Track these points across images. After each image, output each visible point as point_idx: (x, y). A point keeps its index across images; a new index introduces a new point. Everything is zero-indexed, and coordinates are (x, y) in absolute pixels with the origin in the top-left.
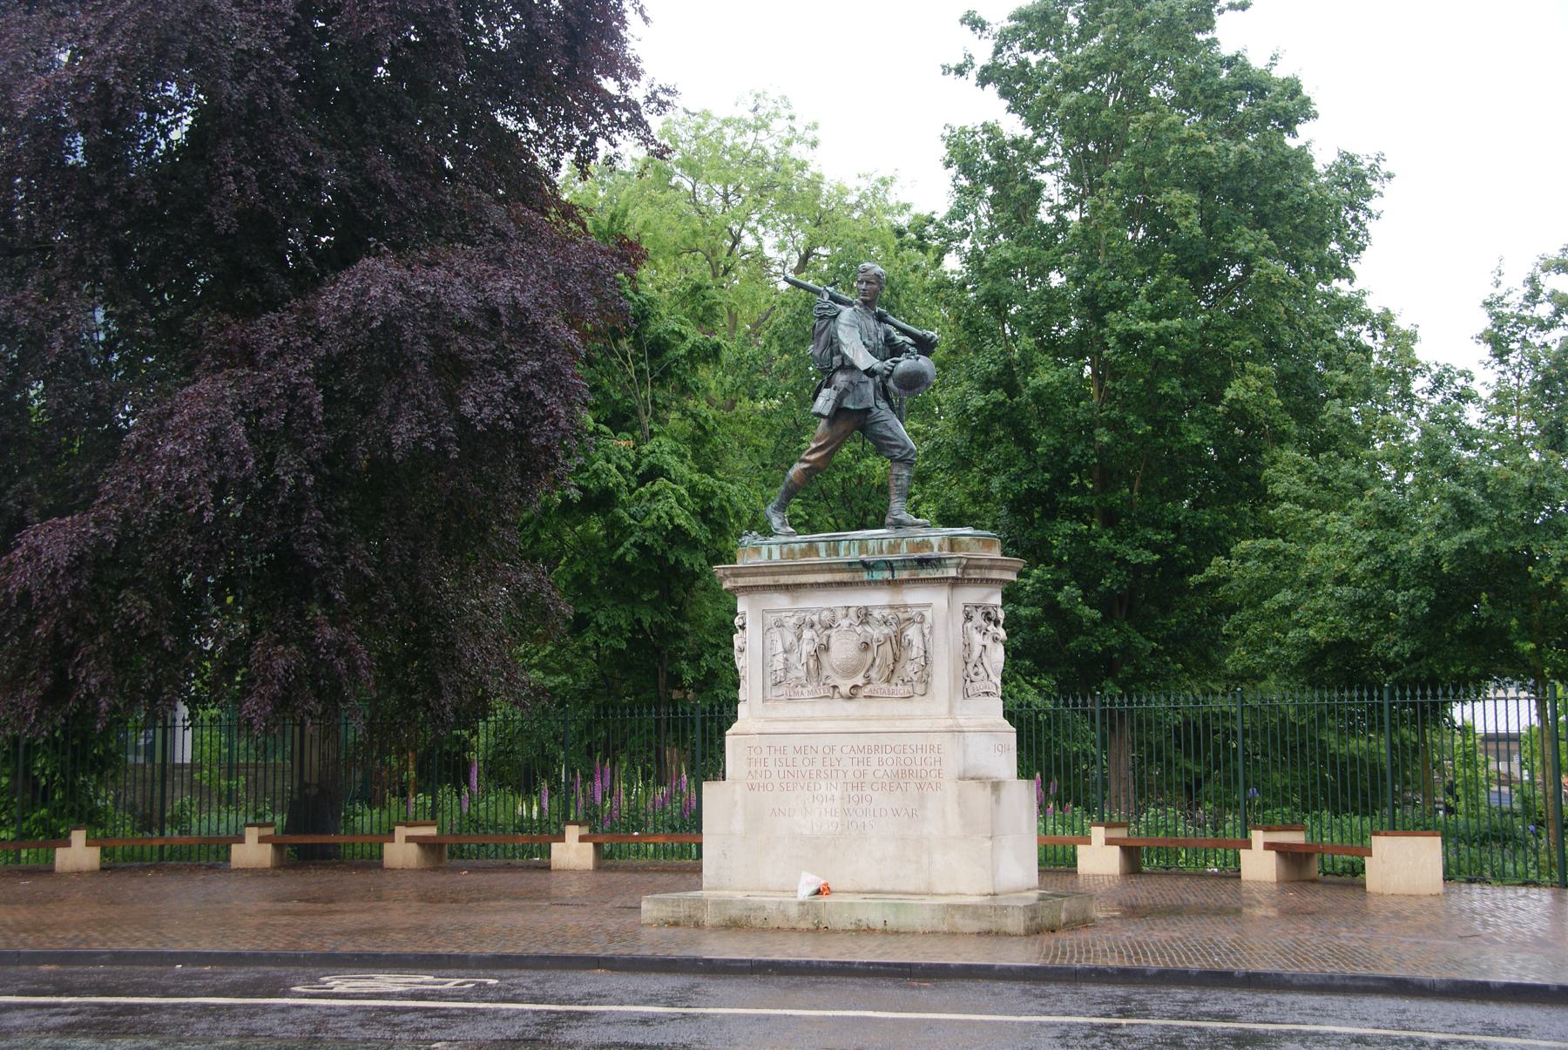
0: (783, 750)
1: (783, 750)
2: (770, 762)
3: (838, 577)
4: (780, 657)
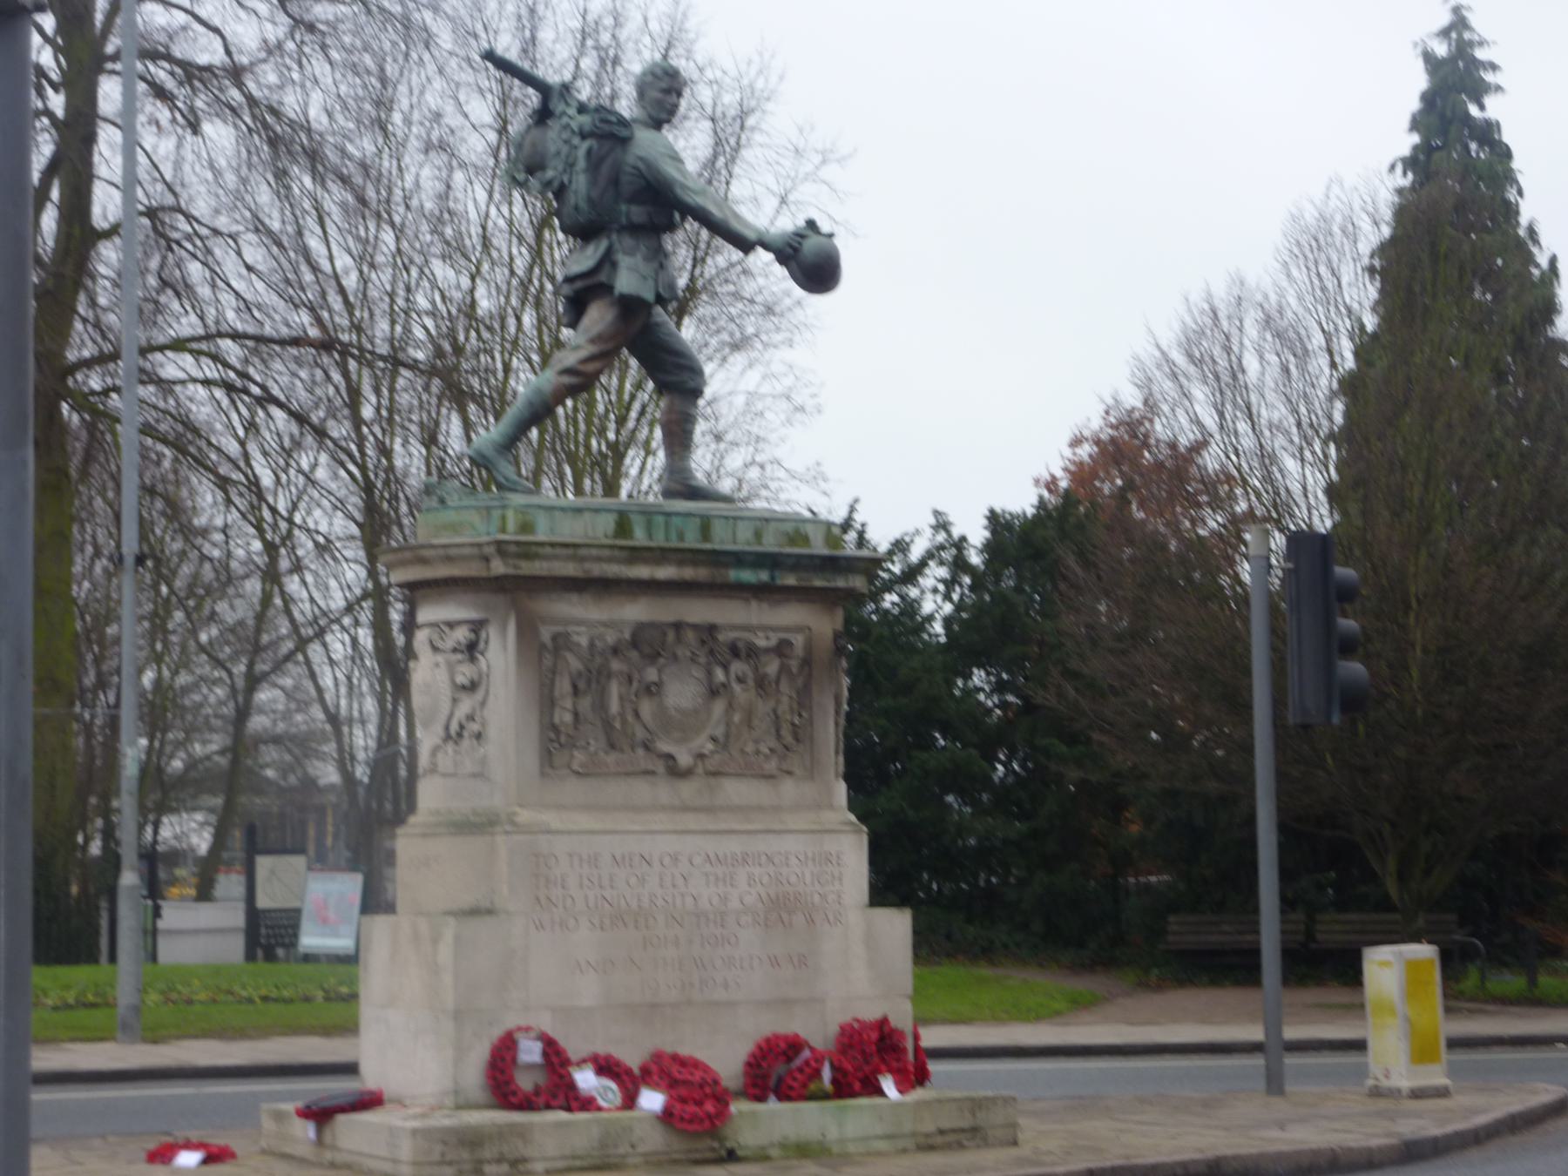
0: (594, 861)
1: (594, 861)
3: (688, 573)
4: (568, 704)
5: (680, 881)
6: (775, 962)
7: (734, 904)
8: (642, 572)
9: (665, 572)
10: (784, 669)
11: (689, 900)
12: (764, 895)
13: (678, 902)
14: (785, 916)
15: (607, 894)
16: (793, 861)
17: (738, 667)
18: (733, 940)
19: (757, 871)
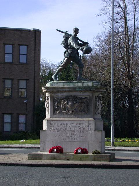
0: (58, 124)
3: (70, 90)
6: (81, 137)
7: (76, 130)
8: (65, 90)
9: (67, 90)
10: (86, 101)
11: (70, 129)
13: (69, 129)
15: (59, 128)
16: (84, 124)
17: (78, 101)
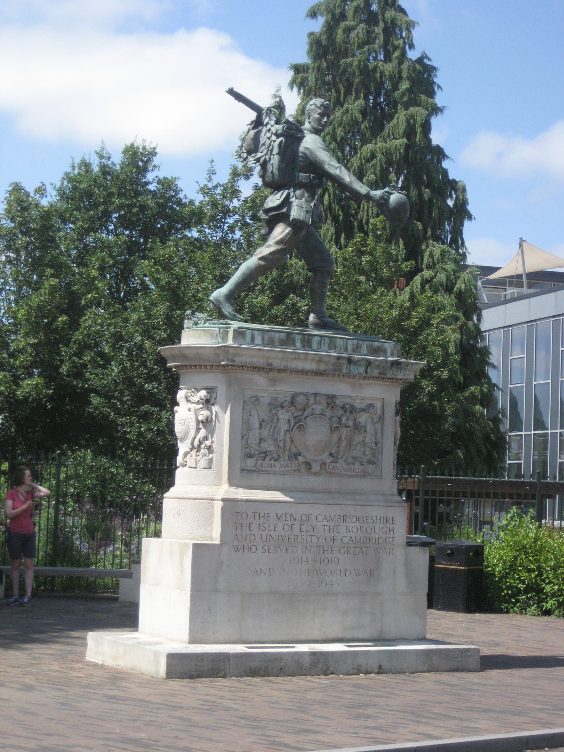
2: (254, 527)
5: (310, 529)
6: (358, 574)
12: (354, 538)
14: (364, 550)
18: (336, 560)
19: (351, 525)
